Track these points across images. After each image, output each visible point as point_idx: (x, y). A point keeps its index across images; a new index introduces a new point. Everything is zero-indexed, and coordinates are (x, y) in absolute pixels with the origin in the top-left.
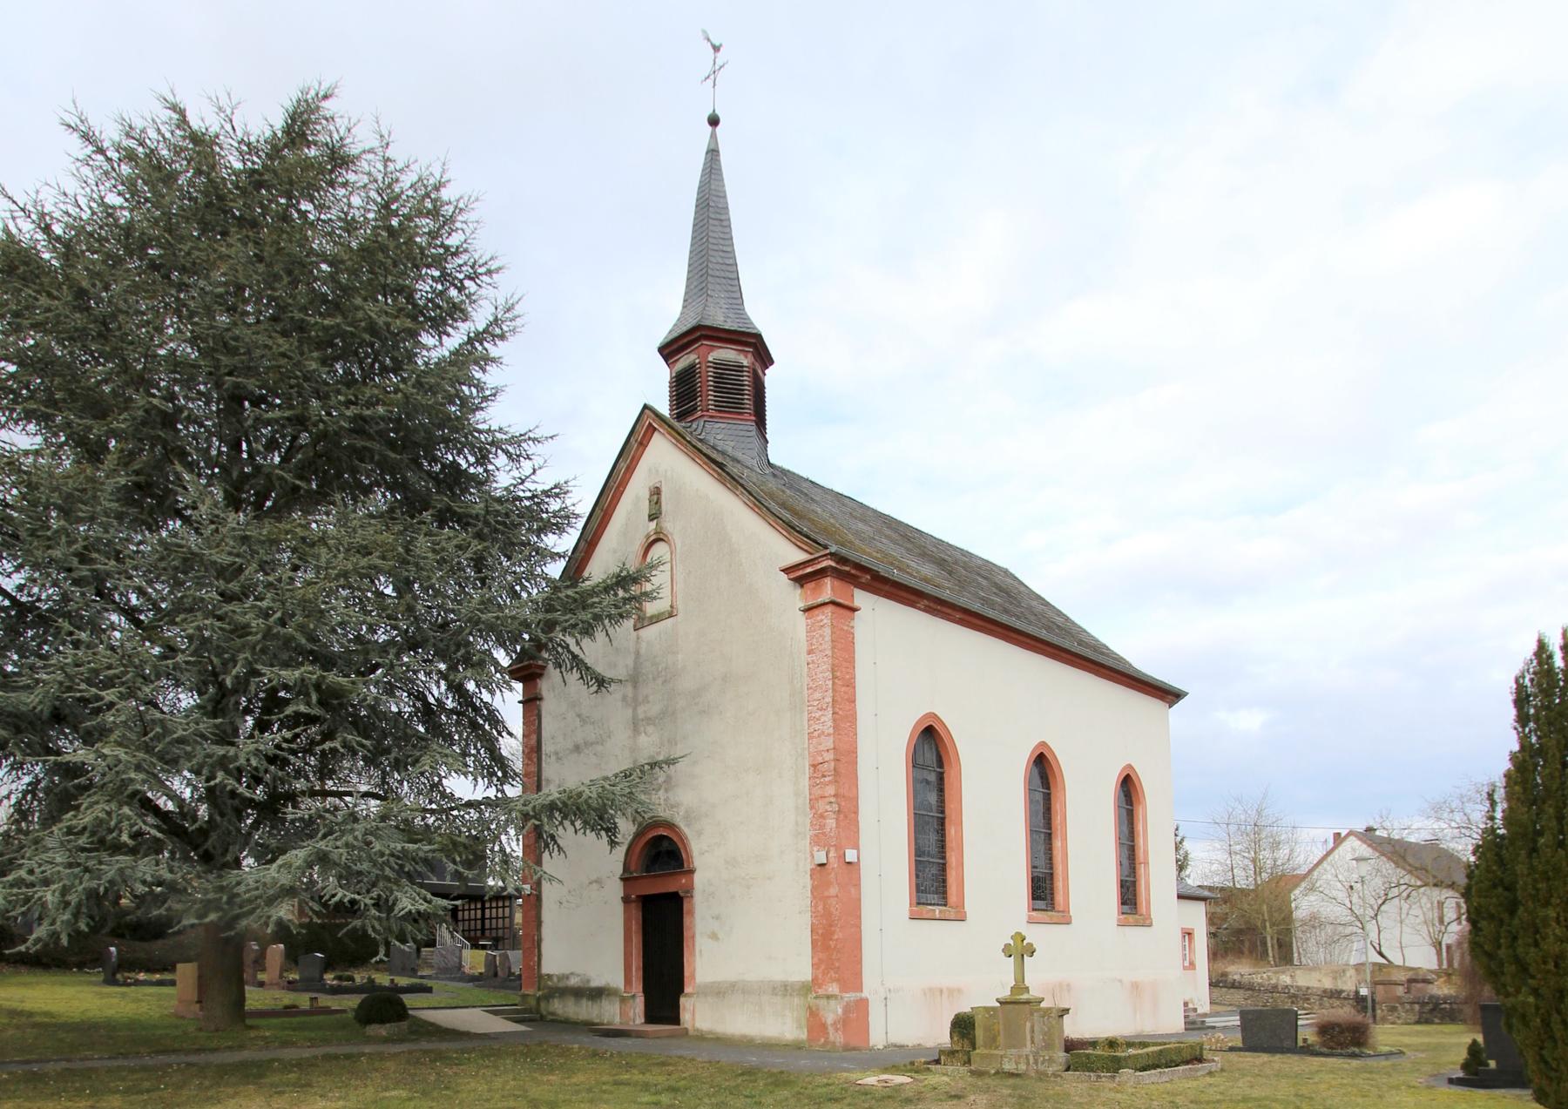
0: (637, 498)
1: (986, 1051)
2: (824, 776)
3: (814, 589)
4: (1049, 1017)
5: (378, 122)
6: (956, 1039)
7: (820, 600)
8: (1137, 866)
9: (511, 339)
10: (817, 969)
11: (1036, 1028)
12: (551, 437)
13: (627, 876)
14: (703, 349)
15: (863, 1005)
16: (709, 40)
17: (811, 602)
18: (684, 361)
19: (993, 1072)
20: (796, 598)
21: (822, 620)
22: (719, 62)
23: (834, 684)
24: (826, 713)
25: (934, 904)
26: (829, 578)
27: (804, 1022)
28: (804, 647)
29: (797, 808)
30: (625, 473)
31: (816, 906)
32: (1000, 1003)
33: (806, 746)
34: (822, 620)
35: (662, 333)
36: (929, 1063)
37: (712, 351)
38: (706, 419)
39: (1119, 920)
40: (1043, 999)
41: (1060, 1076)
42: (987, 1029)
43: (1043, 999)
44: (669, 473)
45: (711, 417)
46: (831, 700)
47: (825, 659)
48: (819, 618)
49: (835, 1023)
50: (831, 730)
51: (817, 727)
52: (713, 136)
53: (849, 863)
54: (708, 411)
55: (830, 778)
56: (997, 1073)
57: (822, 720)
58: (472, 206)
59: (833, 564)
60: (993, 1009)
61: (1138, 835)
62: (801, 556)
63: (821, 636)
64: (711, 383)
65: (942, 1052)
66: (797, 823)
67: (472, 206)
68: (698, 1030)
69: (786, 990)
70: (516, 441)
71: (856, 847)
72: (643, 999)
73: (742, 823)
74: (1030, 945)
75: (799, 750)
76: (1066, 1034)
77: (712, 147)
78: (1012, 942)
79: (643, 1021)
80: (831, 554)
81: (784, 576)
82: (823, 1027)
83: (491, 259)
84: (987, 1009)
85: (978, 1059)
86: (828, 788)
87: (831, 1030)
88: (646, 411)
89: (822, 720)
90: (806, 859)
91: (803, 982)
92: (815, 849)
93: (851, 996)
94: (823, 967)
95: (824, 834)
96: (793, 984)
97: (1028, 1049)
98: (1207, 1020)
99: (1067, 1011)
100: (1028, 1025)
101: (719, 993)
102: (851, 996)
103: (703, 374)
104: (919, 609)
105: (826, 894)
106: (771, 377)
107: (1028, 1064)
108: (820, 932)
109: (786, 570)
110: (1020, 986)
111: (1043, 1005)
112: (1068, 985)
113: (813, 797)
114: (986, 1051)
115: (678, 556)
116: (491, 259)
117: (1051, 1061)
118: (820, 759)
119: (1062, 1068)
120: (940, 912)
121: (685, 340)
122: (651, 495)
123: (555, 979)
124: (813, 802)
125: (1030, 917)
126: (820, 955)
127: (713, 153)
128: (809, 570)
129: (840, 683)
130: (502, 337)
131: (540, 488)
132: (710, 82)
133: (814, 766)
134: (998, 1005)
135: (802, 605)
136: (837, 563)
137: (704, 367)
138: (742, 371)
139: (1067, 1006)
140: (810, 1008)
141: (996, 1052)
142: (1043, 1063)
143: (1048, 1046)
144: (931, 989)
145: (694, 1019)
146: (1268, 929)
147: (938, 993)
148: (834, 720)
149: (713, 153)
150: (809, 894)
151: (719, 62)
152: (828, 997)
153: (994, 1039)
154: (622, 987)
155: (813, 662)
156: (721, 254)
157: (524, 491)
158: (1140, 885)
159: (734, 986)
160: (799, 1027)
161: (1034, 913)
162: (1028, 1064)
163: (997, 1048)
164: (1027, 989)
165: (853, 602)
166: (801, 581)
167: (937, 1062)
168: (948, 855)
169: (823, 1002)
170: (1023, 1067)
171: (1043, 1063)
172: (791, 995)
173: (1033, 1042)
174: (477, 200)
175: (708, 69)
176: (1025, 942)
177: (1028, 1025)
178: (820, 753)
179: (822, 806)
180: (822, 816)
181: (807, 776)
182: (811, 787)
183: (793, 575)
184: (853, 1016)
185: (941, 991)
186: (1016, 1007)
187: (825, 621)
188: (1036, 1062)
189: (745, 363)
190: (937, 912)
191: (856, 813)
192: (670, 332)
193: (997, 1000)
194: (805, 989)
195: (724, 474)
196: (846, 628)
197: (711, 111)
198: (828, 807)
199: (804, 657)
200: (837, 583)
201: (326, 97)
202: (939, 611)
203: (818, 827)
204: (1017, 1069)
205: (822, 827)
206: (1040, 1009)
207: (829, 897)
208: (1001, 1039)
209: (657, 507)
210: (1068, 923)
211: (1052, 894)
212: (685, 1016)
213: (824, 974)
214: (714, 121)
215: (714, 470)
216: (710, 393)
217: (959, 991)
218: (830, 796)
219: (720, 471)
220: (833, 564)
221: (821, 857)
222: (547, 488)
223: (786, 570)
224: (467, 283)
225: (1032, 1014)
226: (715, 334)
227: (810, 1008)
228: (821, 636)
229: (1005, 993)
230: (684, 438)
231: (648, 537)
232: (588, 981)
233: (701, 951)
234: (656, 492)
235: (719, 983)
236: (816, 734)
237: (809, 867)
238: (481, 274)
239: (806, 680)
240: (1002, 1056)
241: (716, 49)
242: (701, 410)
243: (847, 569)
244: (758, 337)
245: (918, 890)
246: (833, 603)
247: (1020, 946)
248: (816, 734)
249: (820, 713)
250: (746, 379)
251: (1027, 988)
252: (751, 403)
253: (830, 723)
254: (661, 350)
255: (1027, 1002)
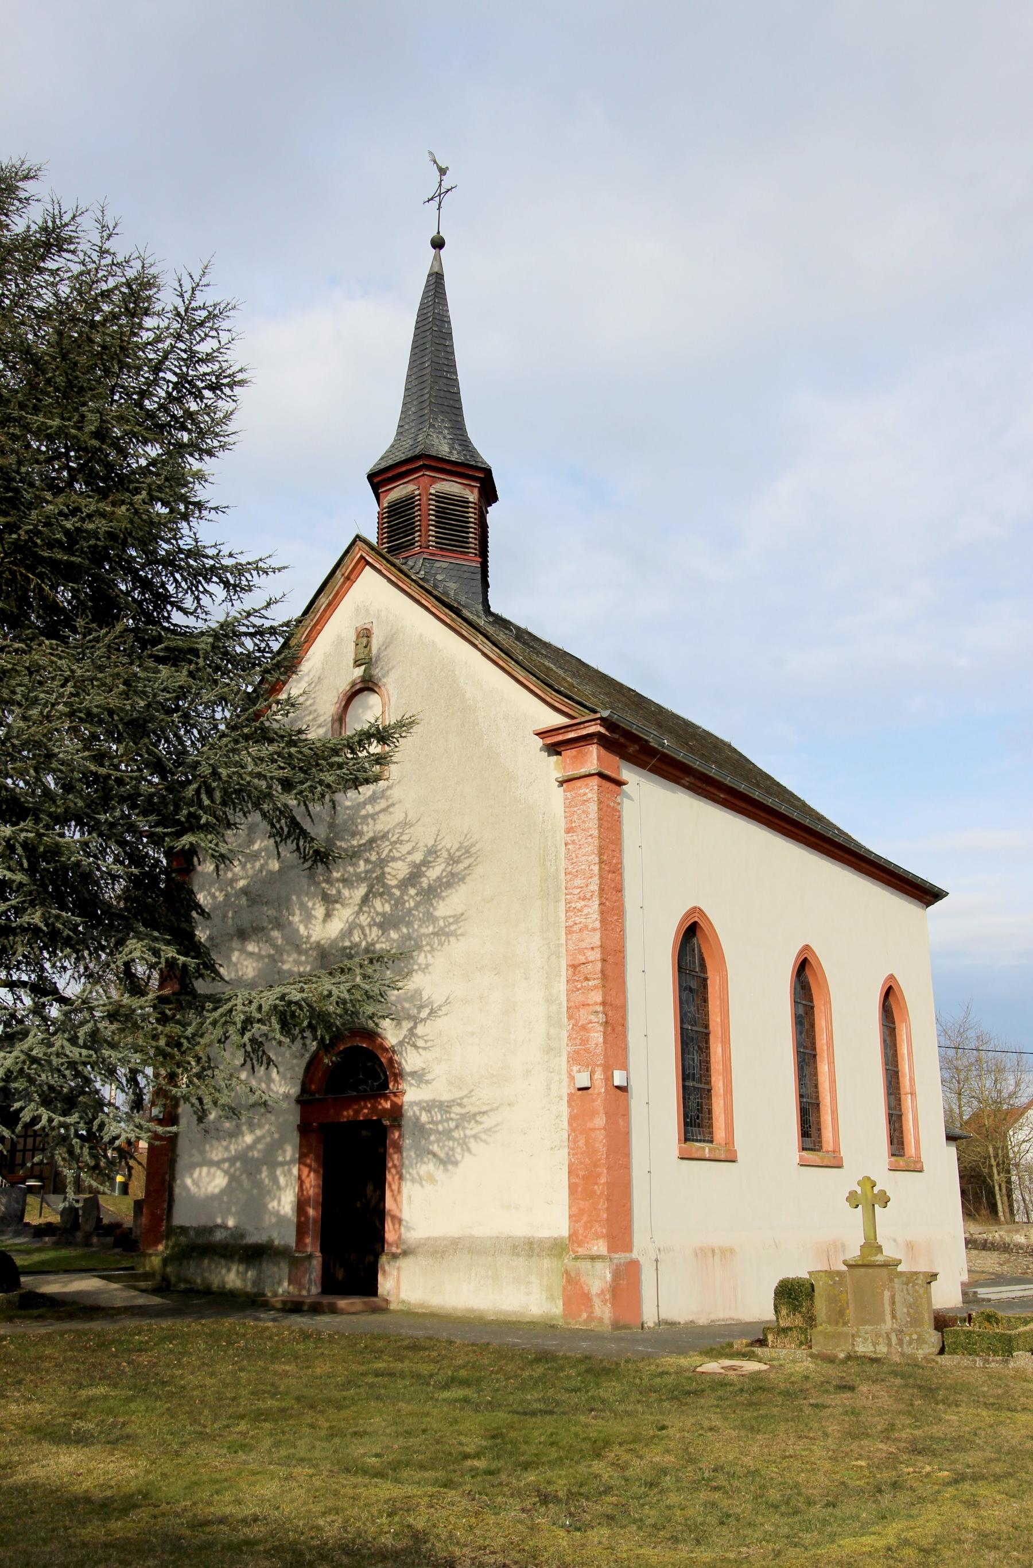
0: (339, 641)
1: (830, 1329)
2: (587, 979)
3: (576, 757)
4: (915, 1284)
5: (103, 212)
6: (784, 1312)
7: (583, 771)
8: (903, 1097)
9: (220, 454)
10: (577, 1221)
11: (897, 1298)
12: (279, 570)
13: (306, 1097)
14: (426, 479)
15: (634, 1266)
16: (435, 162)
17: (571, 773)
18: (398, 492)
19: (842, 1355)
20: (552, 767)
21: (585, 794)
22: (446, 185)
23: (600, 869)
24: (590, 903)
25: (704, 1141)
26: (595, 746)
27: (558, 1291)
28: (562, 823)
29: (549, 1017)
30: (325, 610)
31: (575, 1141)
32: (849, 1266)
33: (563, 941)
34: (585, 794)
35: (370, 463)
36: (751, 1344)
37: (434, 483)
38: (425, 556)
39: (890, 1163)
40: (899, 1262)
41: (933, 1360)
42: (832, 1300)
43: (899, 1262)
44: (383, 614)
45: (431, 554)
46: (597, 888)
47: (590, 839)
48: (582, 791)
49: (602, 1292)
50: (597, 925)
51: (578, 920)
52: (437, 259)
53: (617, 1087)
54: (428, 548)
55: (596, 982)
56: (849, 1358)
57: (585, 911)
58: (228, 314)
59: (602, 730)
60: (839, 1273)
61: (903, 1060)
62: (561, 720)
63: (583, 812)
64: (433, 518)
65: (766, 1330)
66: (549, 1037)
67: (228, 314)
68: (404, 1302)
69: (531, 1249)
70: (240, 570)
71: (624, 1067)
72: (320, 1259)
73: (473, 1034)
74: (883, 1193)
75: (552, 947)
76: (934, 1307)
77: (436, 270)
78: (859, 1190)
79: (320, 1290)
80: (601, 719)
81: (539, 742)
82: (586, 1298)
83: (240, 371)
84: (830, 1274)
85: (821, 1339)
86: (592, 993)
87: (597, 1302)
88: (358, 543)
89: (585, 911)
90: (560, 1081)
91: (555, 1239)
92: (575, 1068)
93: (620, 1257)
94: (585, 1219)
95: (587, 1050)
96: (541, 1241)
97: (888, 1324)
98: (980, 1290)
99: (934, 1276)
100: (887, 1294)
101: (436, 1252)
102: (620, 1257)
103: (423, 508)
104: (684, 786)
105: (590, 1125)
106: (494, 514)
107: (889, 1345)
108: (581, 1173)
109: (541, 734)
110: (872, 1245)
111: (900, 1268)
112: (843, 1245)
113: (572, 1004)
114: (830, 1329)
115: (392, 710)
116: (240, 371)
117: (921, 1340)
118: (583, 959)
119: (936, 1350)
120: (710, 1150)
121: (403, 469)
122: (358, 637)
123: (192, 1233)
124: (572, 1011)
125: (801, 1158)
126: (582, 1204)
127: (436, 282)
128: (572, 735)
129: (607, 868)
130: (210, 453)
131: (267, 624)
132: (434, 204)
133: (574, 967)
134: (844, 1268)
135: (559, 775)
136: (607, 729)
137: (424, 499)
138: (468, 507)
139: (935, 1271)
140: (567, 1272)
141: (845, 1329)
142: (910, 1343)
143: (915, 1321)
144: (701, 1249)
145: (398, 1288)
146: (996, 1177)
147: (710, 1254)
148: (602, 913)
149: (436, 282)
150: (566, 1125)
151: (446, 185)
152: (593, 1258)
153: (841, 1313)
154: (293, 1245)
155: (573, 842)
156: (445, 381)
157: (248, 627)
158: (908, 1120)
159: (457, 1244)
160: (551, 1298)
161: (804, 1153)
162: (889, 1345)
163: (845, 1324)
164: (879, 1249)
165: (619, 774)
166: (554, 749)
167: (762, 1342)
168: (713, 1079)
169: (585, 1265)
170: (882, 1349)
171: (910, 1343)
172: (538, 1256)
173: (894, 1317)
174: (234, 308)
175: (447, 199)
176: (876, 1190)
177: (887, 1294)
178: (581, 951)
179: (584, 1016)
180: (584, 1028)
181: (564, 979)
182: (569, 992)
183: (549, 741)
184: (623, 1283)
185: (713, 1251)
186: (870, 1270)
187: (590, 795)
188: (900, 1342)
189: (471, 500)
190: (707, 1150)
191: (624, 1025)
192: (382, 458)
193: (845, 1263)
194: (557, 1248)
195: (460, 620)
196: (612, 804)
197: (435, 233)
198: (593, 1018)
199: (561, 836)
200: (603, 751)
201: (26, 178)
202: (703, 789)
203: (578, 1042)
204: (875, 1352)
205: (584, 1041)
206: (901, 1273)
207: (594, 1129)
208: (850, 1313)
209: (367, 650)
210: (840, 1167)
211: (819, 1129)
212: (386, 1284)
213: (585, 1228)
214: (438, 244)
215: (446, 614)
216: (431, 528)
217: (732, 1251)
218: (596, 1004)
219: (454, 616)
220: (602, 730)
221: (583, 1080)
222: (275, 624)
223: (541, 734)
224: (207, 393)
225: (891, 1280)
226: (433, 464)
227: (567, 1272)
228: (583, 812)
229: (854, 1252)
230: (408, 576)
231: (353, 685)
232: (242, 1236)
233: (410, 1197)
234: (365, 635)
235: (436, 1239)
236: (576, 928)
237: (565, 1092)
238: (223, 384)
239: (563, 864)
240: (853, 1336)
241: (443, 171)
242: (420, 546)
243: (616, 736)
244: (488, 472)
245: (686, 1124)
246: (601, 775)
247: (869, 1195)
248: (576, 928)
249: (583, 903)
250: (472, 517)
251: (880, 1247)
252: (477, 542)
253: (596, 916)
254: (371, 477)
255: (885, 1265)
